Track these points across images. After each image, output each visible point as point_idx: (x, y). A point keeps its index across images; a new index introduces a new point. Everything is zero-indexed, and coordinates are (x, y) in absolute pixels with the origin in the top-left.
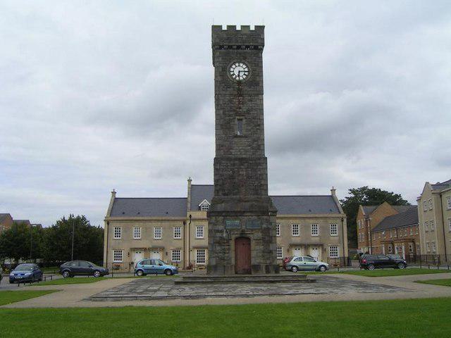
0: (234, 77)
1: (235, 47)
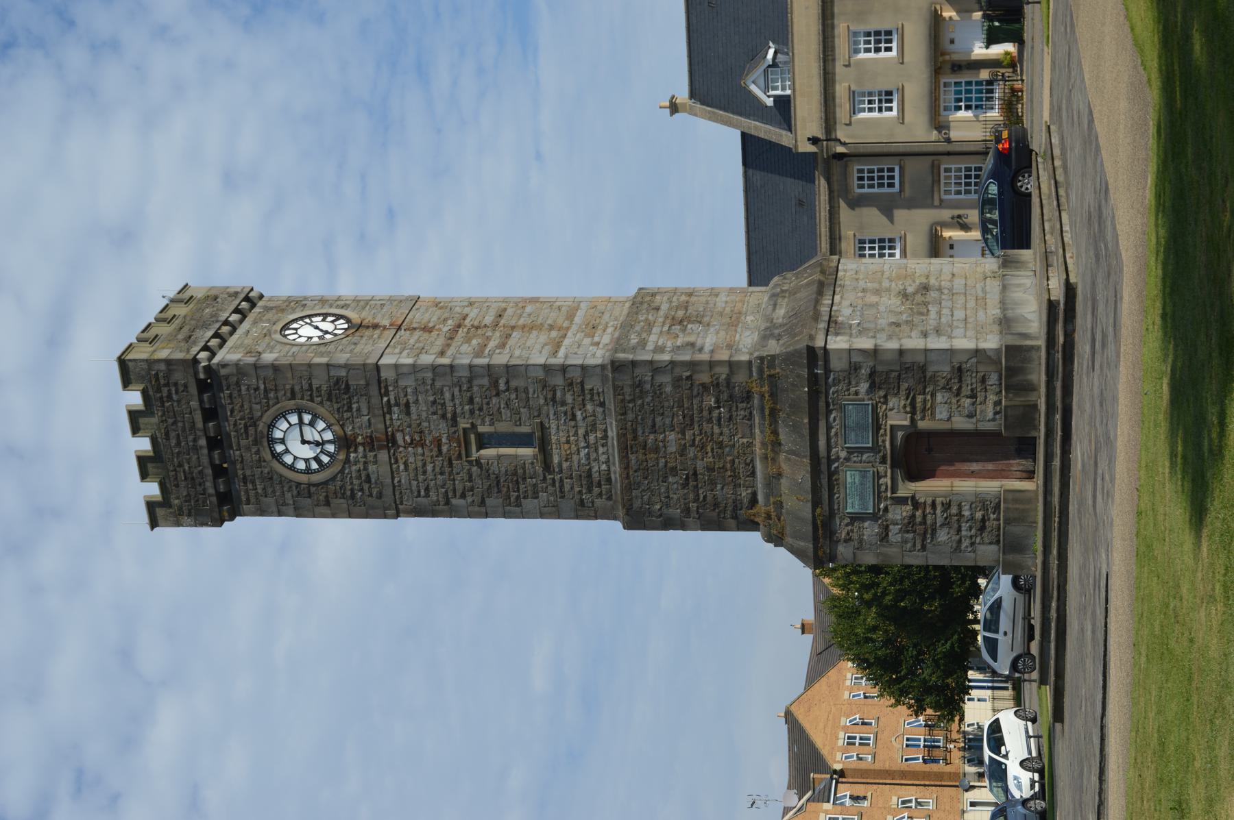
0: (325, 459)
1: (216, 454)
